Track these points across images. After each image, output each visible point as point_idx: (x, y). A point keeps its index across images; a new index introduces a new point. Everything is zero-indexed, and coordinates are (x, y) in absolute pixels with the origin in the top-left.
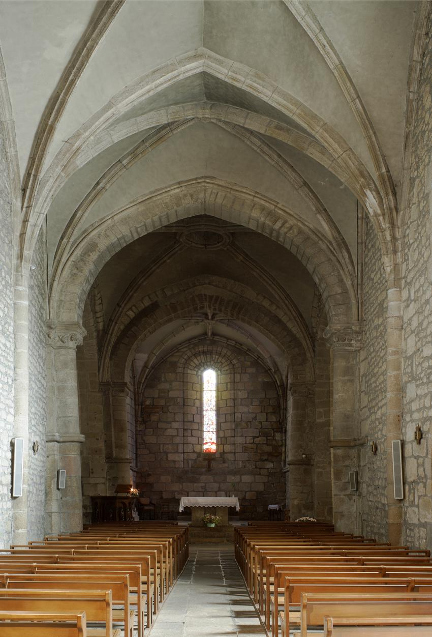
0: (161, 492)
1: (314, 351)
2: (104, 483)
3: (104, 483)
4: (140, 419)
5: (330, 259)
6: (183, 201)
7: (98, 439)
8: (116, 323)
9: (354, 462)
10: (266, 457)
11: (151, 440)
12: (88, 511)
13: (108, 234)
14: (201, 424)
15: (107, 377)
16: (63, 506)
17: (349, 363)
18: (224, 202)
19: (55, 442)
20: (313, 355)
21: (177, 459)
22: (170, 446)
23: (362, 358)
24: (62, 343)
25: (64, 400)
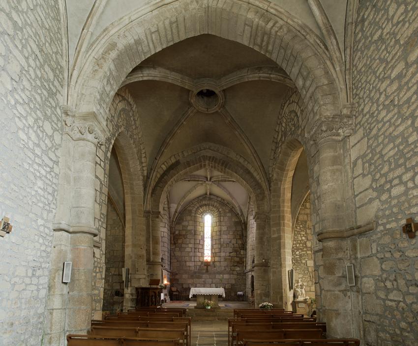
0: (182, 284)
1: (270, 190)
2: (145, 278)
3: (145, 278)
4: (173, 242)
5: (316, 54)
6: (190, 6)
7: (141, 248)
8: (154, 171)
9: (347, 254)
10: (236, 264)
11: (178, 254)
12: (134, 297)
13: (126, 35)
14: (203, 245)
15: (149, 208)
16: (69, 301)
17: (336, 152)
18: (225, 6)
19: (63, 232)
20: (269, 193)
21: (191, 265)
22: (187, 258)
23: (352, 144)
24: (81, 135)
25: (79, 189)
